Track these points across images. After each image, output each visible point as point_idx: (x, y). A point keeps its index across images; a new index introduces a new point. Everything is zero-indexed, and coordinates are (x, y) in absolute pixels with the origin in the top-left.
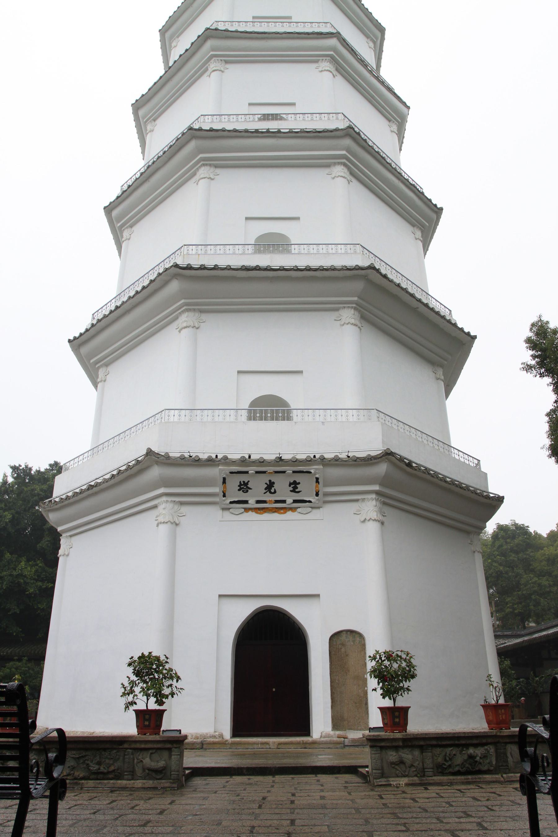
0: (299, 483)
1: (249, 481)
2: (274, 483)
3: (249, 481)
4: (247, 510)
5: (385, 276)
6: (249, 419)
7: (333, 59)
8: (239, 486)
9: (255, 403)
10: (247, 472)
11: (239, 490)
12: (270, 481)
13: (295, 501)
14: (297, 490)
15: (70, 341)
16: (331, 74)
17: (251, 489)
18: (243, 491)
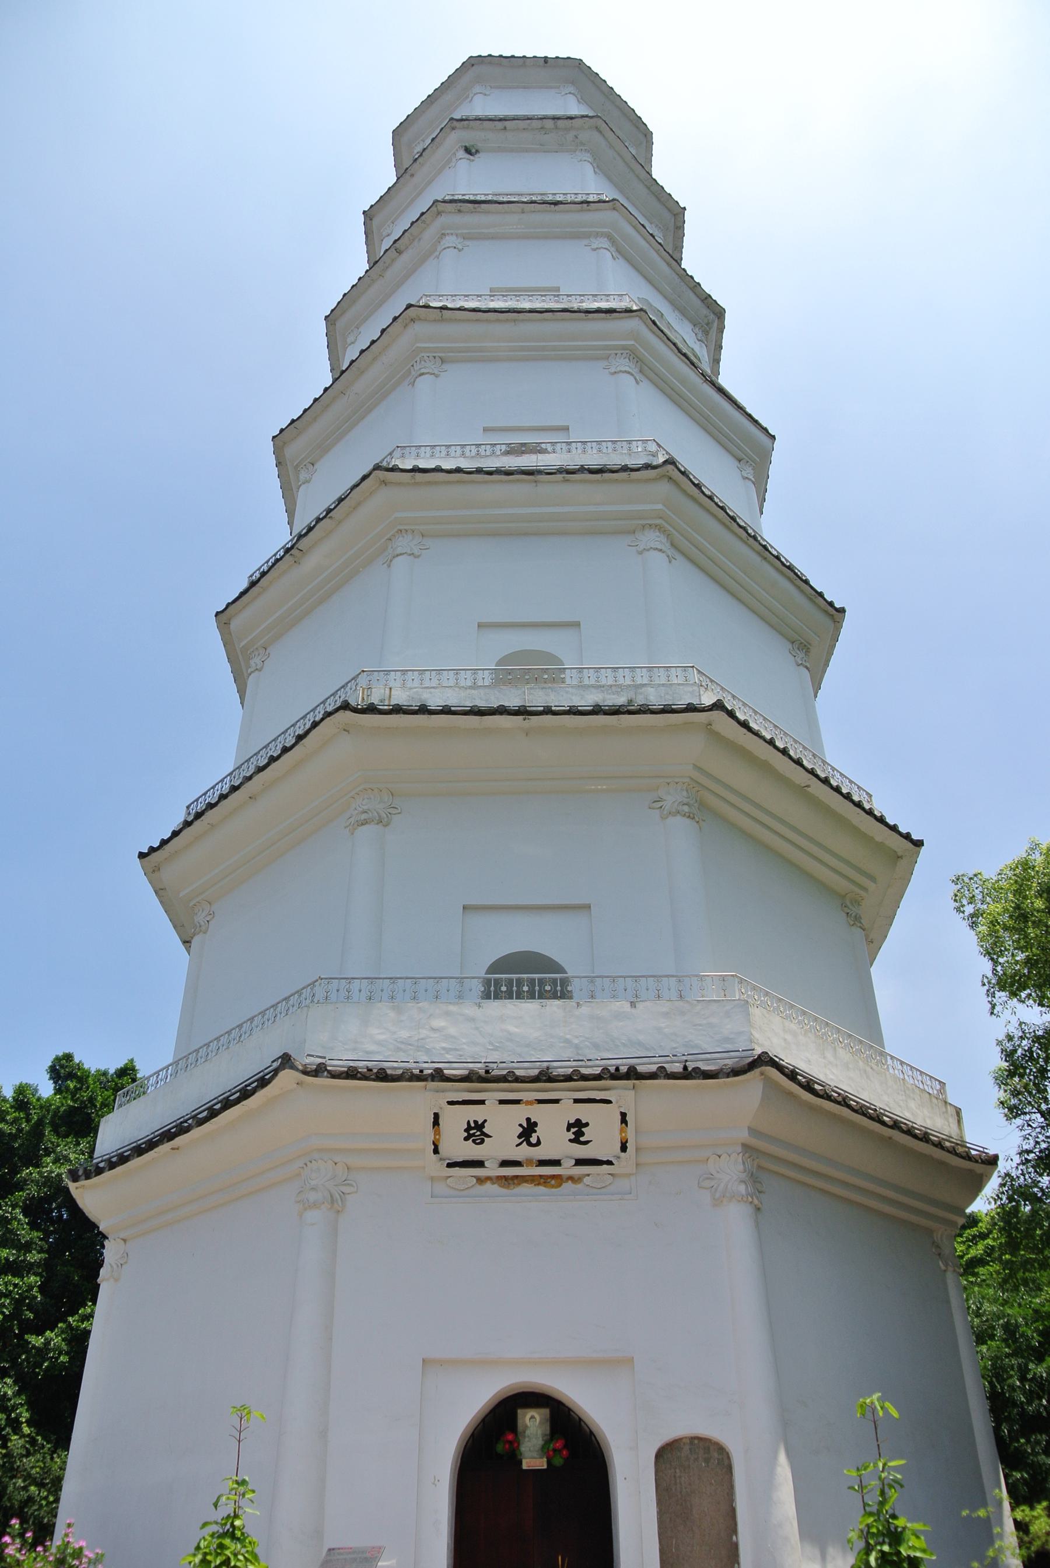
0: (587, 1125)
1: (485, 1121)
2: (535, 1124)
3: (485, 1121)
4: (480, 1180)
5: (745, 725)
6: (487, 996)
7: (633, 355)
8: (465, 1131)
9: (497, 967)
10: (482, 1102)
11: (466, 1139)
12: (528, 1120)
13: (579, 1162)
14: (582, 1139)
15: (142, 856)
16: (632, 378)
17: (489, 1136)
18: (474, 1141)
